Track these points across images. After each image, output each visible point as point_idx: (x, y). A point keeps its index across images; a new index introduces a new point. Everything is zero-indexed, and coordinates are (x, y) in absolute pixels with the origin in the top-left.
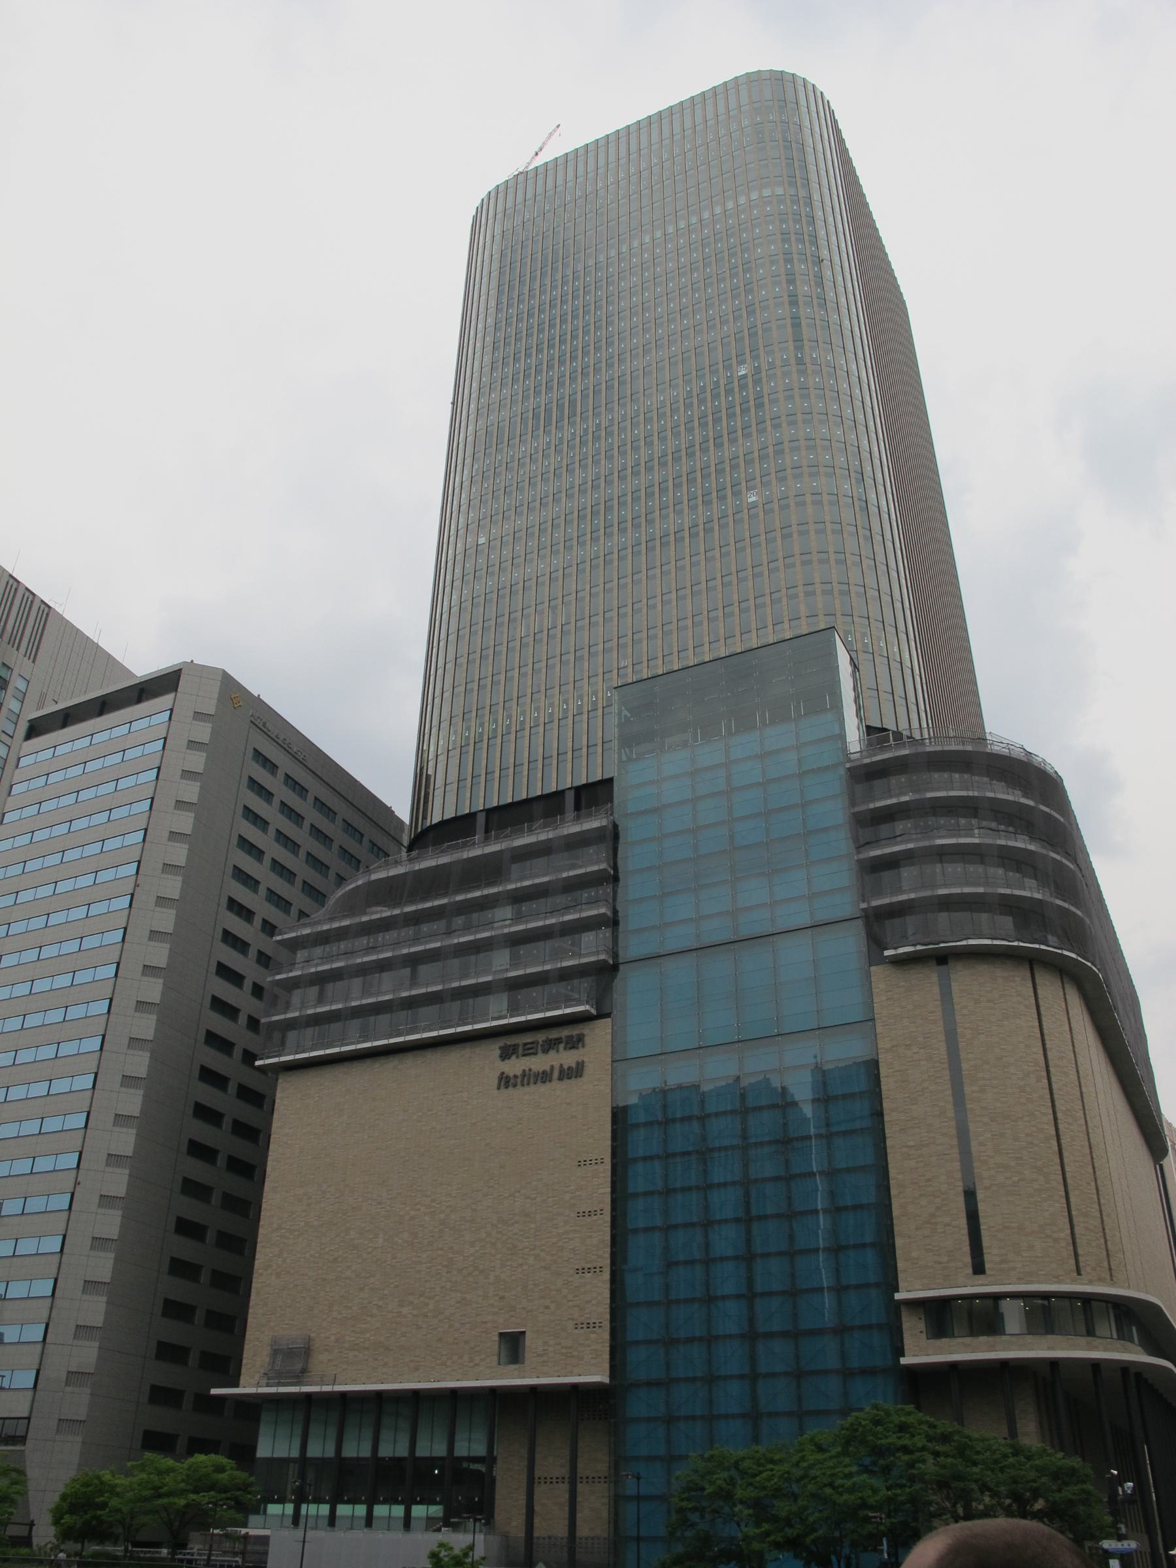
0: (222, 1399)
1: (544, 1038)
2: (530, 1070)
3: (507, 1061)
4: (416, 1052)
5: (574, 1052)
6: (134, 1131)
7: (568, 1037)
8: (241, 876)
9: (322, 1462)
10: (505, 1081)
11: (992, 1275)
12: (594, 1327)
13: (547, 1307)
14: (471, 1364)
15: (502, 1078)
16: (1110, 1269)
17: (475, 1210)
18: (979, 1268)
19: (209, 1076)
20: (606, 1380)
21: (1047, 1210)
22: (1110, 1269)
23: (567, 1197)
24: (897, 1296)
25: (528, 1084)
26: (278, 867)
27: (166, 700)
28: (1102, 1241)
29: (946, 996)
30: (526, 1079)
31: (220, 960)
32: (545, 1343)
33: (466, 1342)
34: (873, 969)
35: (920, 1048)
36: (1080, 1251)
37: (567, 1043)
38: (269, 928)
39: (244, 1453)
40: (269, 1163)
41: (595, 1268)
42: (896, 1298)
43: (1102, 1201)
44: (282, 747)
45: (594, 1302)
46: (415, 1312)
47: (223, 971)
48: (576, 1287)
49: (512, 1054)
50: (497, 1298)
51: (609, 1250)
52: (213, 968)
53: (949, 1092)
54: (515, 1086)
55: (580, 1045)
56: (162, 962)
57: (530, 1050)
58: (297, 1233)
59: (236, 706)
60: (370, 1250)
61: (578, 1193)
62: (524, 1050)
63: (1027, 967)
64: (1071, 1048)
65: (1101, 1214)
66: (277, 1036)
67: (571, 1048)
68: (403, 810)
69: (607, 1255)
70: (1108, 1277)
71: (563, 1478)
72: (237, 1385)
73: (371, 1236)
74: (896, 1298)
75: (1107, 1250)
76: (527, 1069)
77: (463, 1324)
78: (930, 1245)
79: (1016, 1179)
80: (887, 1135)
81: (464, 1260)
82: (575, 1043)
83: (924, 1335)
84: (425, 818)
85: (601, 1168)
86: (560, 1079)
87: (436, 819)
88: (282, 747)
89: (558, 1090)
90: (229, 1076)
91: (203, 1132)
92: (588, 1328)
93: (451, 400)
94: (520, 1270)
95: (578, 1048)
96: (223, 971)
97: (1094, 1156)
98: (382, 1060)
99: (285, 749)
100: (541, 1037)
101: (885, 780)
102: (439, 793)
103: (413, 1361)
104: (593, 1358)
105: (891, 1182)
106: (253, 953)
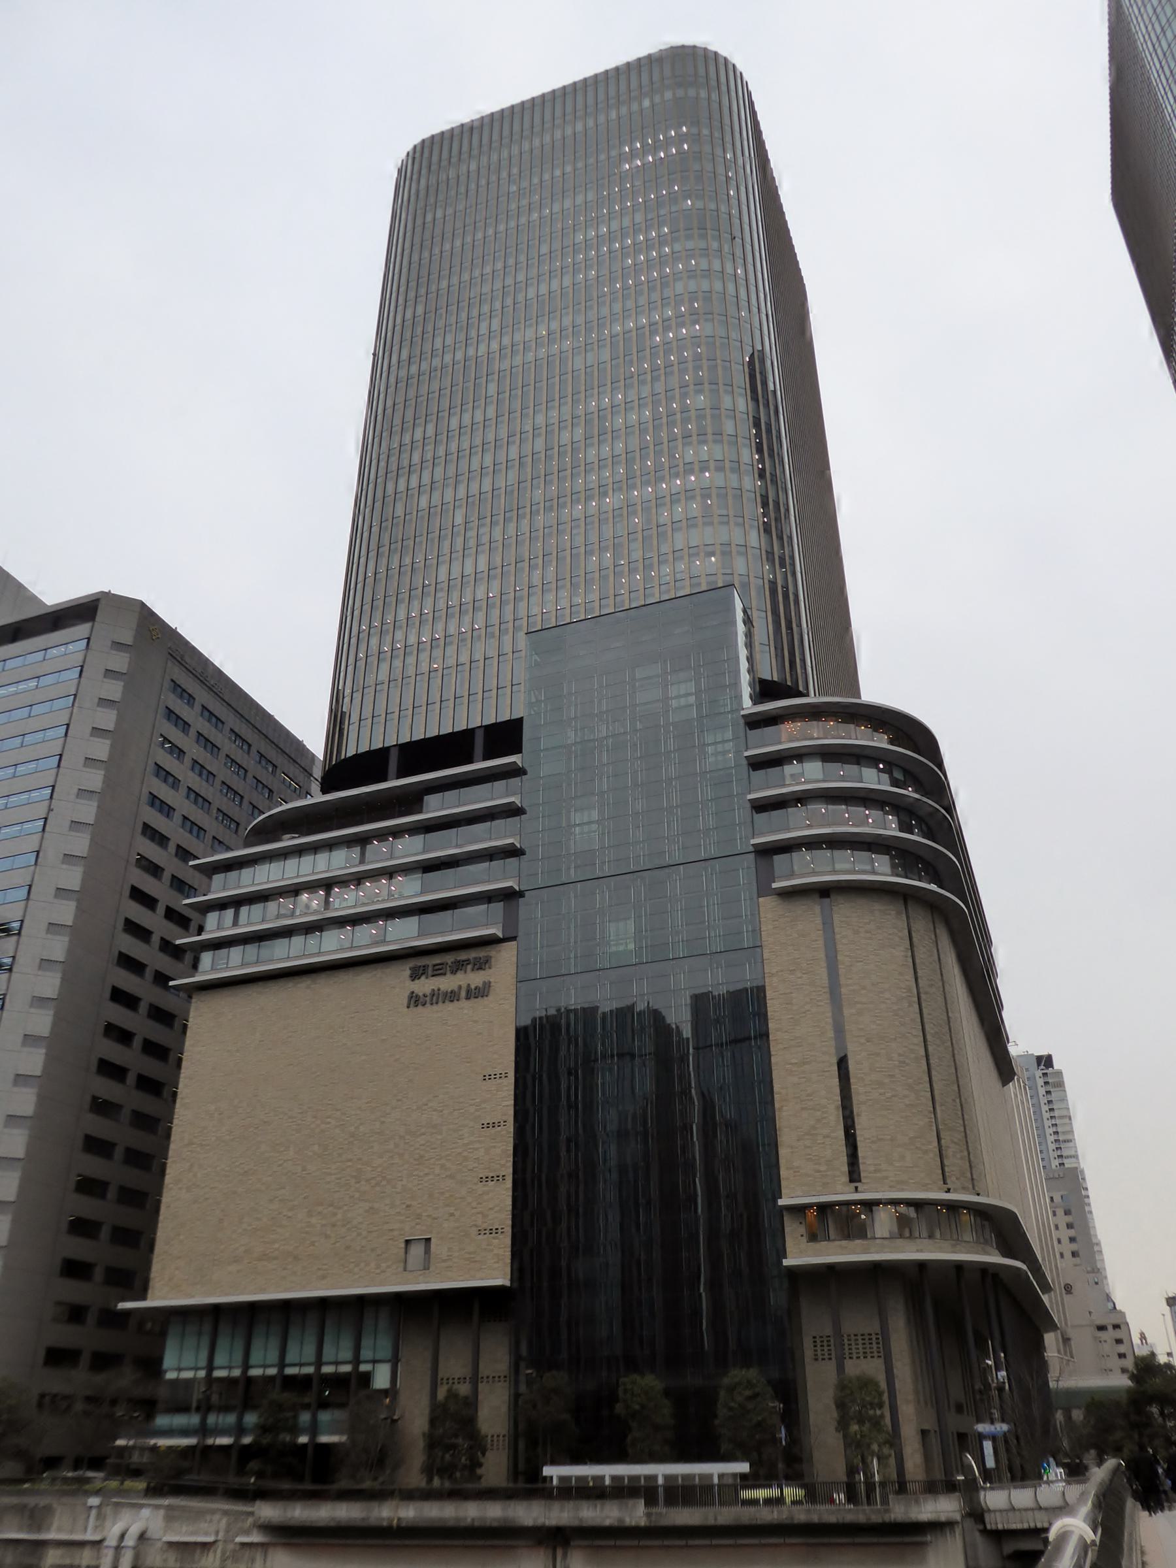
0: (128, 1313)
1: (453, 960)
2: (439, 990)
3: (417, 981)
4: (328, 972)
5: (482, 972)
6: (43, 1051)
7: (475, 958)
8: (150, 832)
9: (230, 1382)
10: (415, 1000)
11: (867, 1183)
12: (496, 1233)
13: (452, 1215)
14: (378, 1271)
15: (412, 997)
16: (972, 1179)
17: (383, 1122)
18: (854, 1175)
19: (119, 996)
20: (508, 1283)
21: (917, 1124)
22: (972, 1179)
23: (472, 1109)
24: (781, 1202)
25: (437, 1003)
26: (194, 795)
27: (83, 629)
28: (966, 1153)
29: (828, 926)
30: (435, 998)
31: (128, 916)
32: (450, 1249)
33: (373, 1250)
34: (761, 899)
35: (804, 974)
36: (946, 1162)
37: (475, 965)
38: (184, 854)
39: (152, 1366)
40: (181, 1080)
41: (498, 1177)
42: (784, 1264)
43: (966, 1116)
44: (199, 679)
45: (497, 1209)
46: (324, 1222)
47: (137, 894)
48: (480, 1195)
49: (422, 974)
50: (404, 1206)
51: (511, 1159)
52: (127, 892)
53: (830, 1014)
54: (424, 1005)
55: (487, 966)
56: (117, 696)
57: (439, 971)
58: (208, 1147)
59: (154, 638)
60: (280, 1162)
61: (483, 1106)
62: (434, 970)
63: (902, 902)
64: (940, 977)
65: (965, 1129)
66: (188, 957)
67: (478, 969)
68: (316, 744)
69: (510, 1164)
70: (971, 1186)
71: (465, 1378)
72: (144, 1298)
73: (282, 1149)
74: (784, 1264)
75: (970, 1161)
76: (436, 989)
77: (369, 1232)
78: (810, 1155)
79: (888, 1095)
80: (772, 1053)
81: (373, 1171)
82: (481, 965)
83: (804, 1239)
84: (339, 752)
85: (505, 1081)
86: (468, 998)
87: (351, 752)
88: (199, 679)
89: (464, 1007)
90: (134, 1031)
91: (101, 1128)
92: (491, 1233)
93: (372, 351)
94: (426, 1179)
95: (484, 970)
96: (137, 894)
97: (959, 1075)
98: (297, 979)
99: (201, 681)
100: (449, 958)
101: (788, 855)
102: (354, 728)
103: (319, 1269)
104: (495, 1263)
105: (776, 1096)
106: (161, 909)
